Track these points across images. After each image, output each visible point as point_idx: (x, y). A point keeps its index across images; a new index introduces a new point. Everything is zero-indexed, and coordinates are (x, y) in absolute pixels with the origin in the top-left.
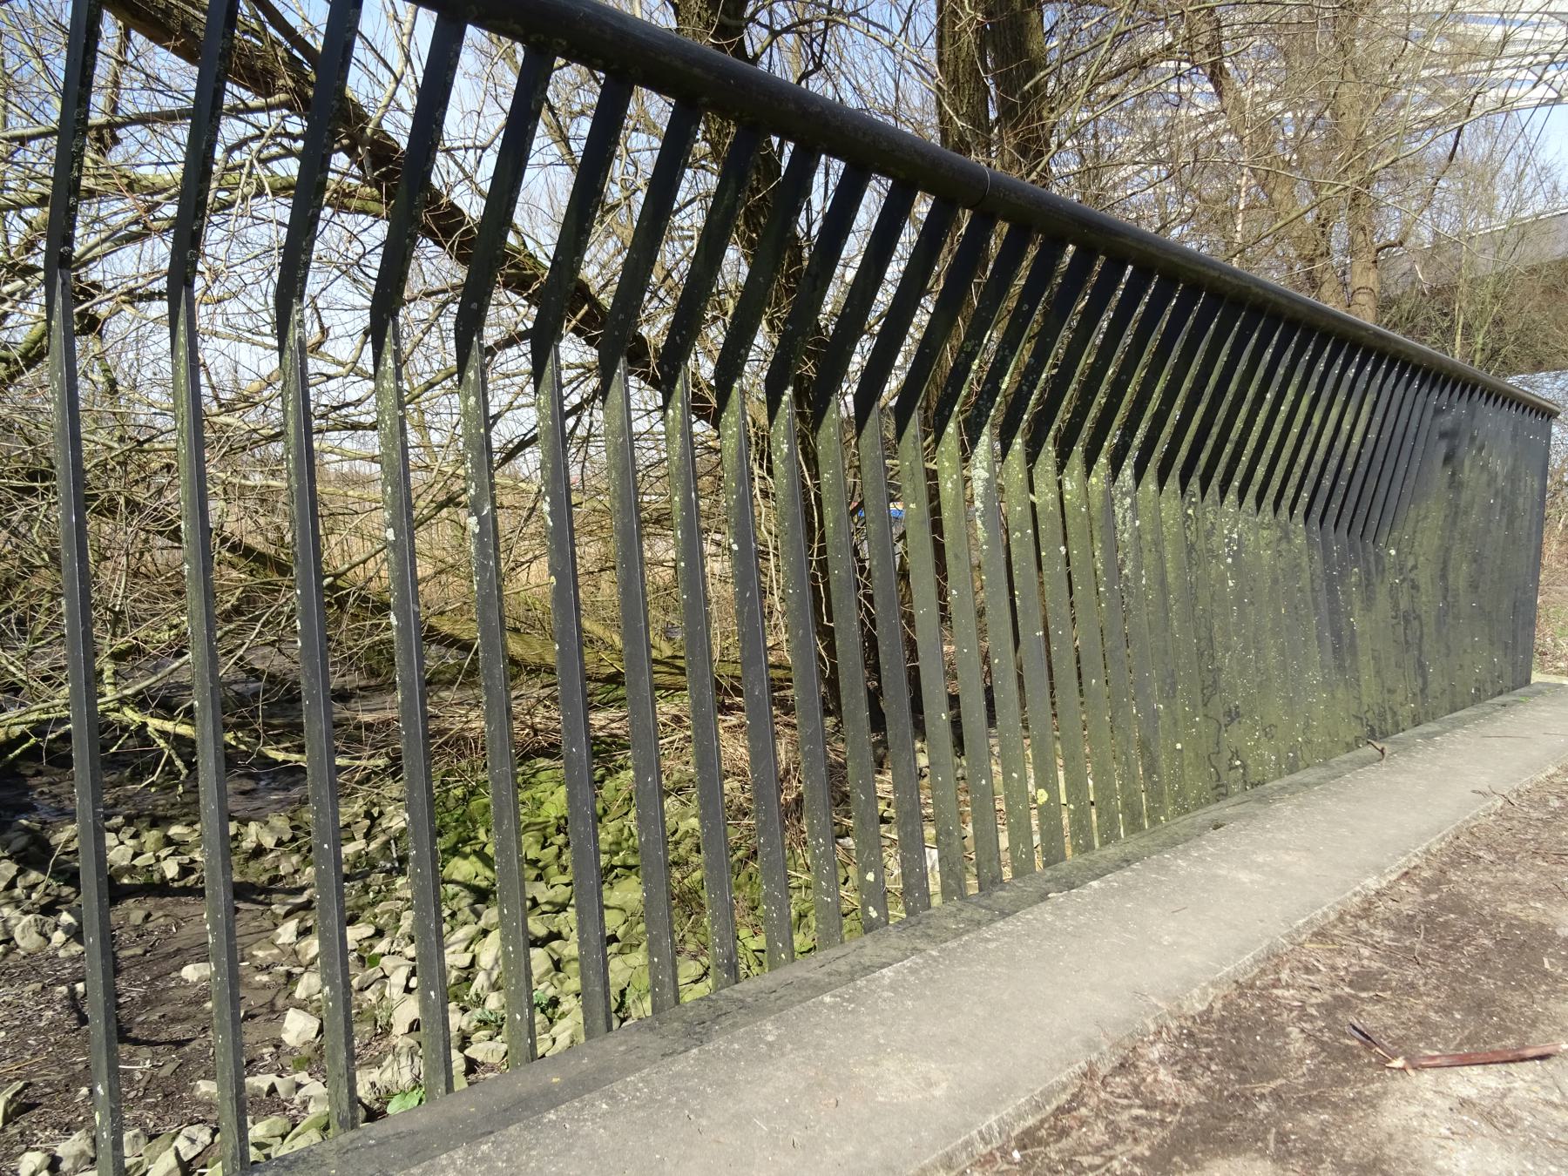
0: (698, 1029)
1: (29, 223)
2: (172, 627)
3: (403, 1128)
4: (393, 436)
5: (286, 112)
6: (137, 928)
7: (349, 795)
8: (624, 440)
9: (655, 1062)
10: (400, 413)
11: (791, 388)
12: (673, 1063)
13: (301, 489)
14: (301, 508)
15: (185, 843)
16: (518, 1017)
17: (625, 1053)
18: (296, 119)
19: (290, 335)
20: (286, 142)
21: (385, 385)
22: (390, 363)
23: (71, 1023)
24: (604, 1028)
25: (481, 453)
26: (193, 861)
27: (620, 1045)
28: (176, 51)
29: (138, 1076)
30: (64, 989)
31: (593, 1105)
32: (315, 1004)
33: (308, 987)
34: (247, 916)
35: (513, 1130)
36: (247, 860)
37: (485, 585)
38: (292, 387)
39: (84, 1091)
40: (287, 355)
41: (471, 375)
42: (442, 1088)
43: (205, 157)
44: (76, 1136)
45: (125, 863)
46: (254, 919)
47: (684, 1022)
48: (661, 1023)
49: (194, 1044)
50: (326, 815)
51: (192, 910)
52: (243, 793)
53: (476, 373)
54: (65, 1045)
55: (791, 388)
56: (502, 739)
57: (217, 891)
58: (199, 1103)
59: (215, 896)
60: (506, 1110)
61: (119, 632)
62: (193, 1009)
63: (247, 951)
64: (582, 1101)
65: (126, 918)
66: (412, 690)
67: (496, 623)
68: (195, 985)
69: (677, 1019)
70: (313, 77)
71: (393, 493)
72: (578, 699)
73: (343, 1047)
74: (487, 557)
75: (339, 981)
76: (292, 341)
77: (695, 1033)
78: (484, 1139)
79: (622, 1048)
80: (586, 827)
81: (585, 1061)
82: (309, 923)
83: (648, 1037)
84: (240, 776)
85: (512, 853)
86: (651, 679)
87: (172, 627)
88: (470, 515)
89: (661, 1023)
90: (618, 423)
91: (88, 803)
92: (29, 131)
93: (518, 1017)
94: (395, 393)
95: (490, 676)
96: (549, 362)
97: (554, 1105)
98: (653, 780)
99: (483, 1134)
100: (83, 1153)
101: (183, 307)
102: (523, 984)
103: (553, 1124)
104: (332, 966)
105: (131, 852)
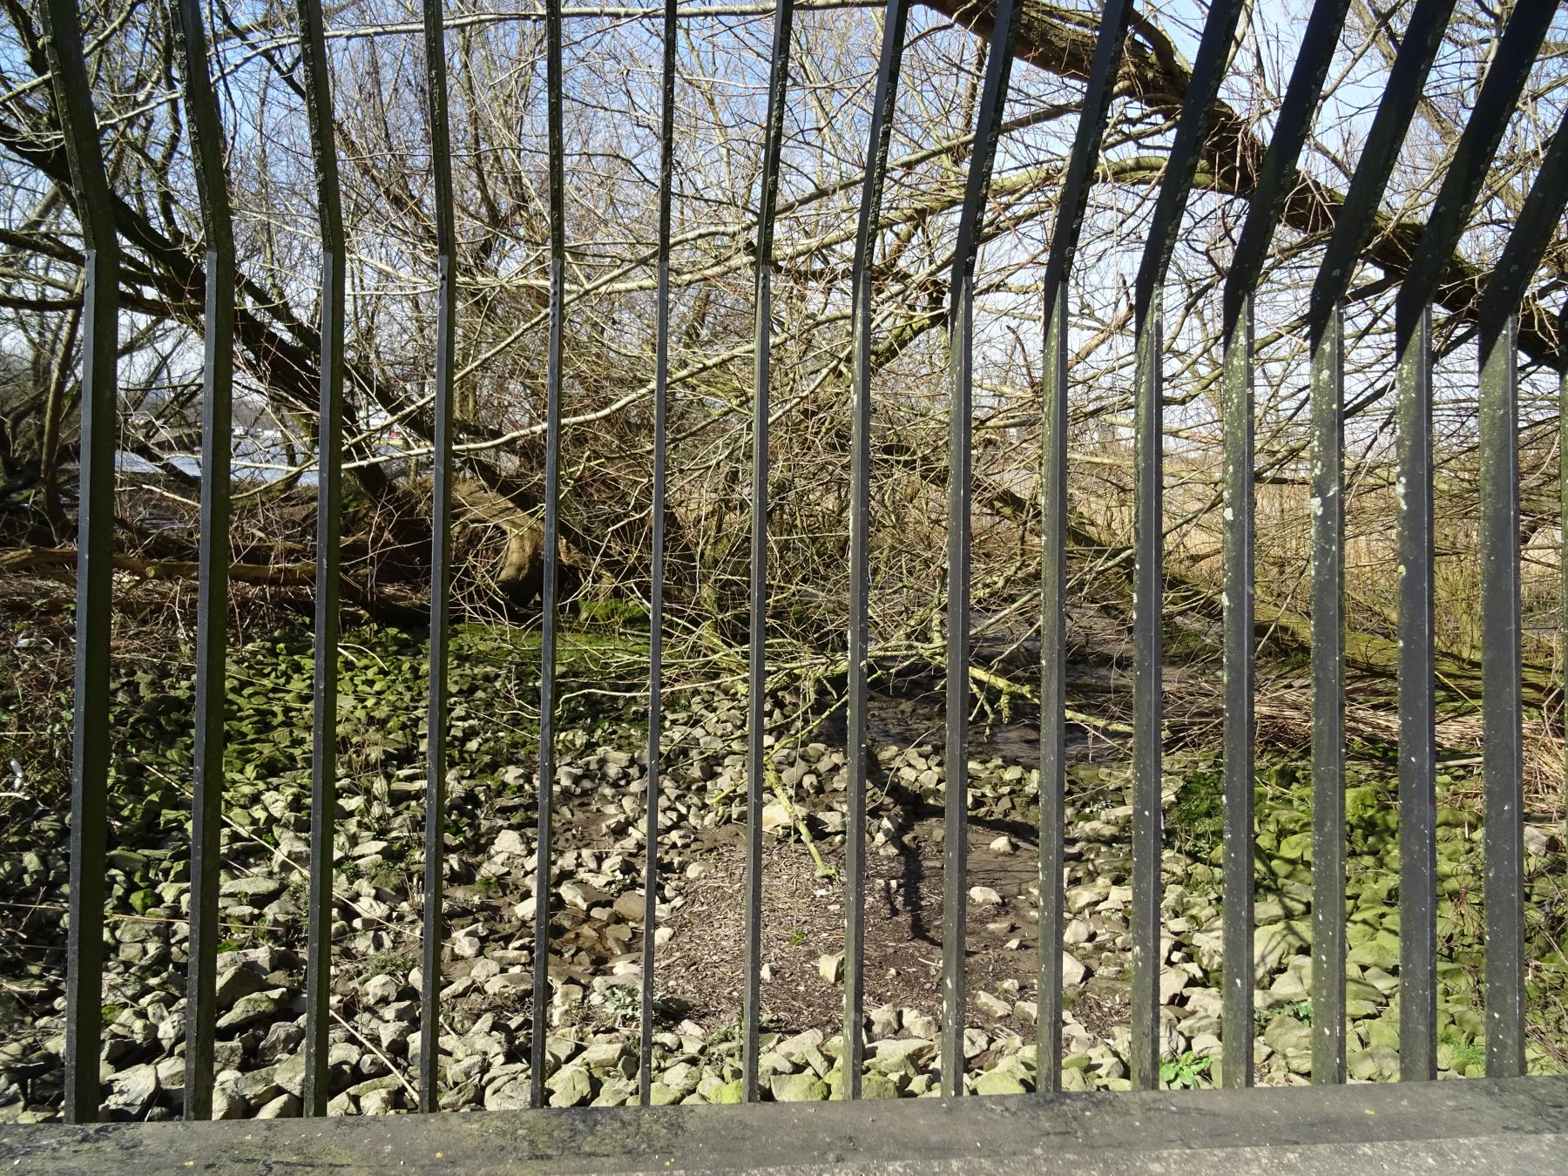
0: (1552, 1111)
1: (897, 235)
2: (986, 586)
3: (1203, 1105)
4: (1240, 414)
5: (1127, 99)
6: (937, 844)
7: (1122, 760)
8: (1506, 413)
9: (1494, 1132)
10: (1249, 391)
11: (119, 236)
12: (1520, 1141)
13: (1147, 468)
14: (1147, 486)
15: (978, 778)
16: (1327, 1032)
17: (1454, 1109)
18: (1137, 104)
19: (1148, 319)
20: (1125, 128)
21: (1235, 362)
22: (1242, 340)
23: (885, 912)
24: (1426, 1074)
25: (1332, 431)
26: (984, 795)
27: (1449, 1098)
28: (1035, 62)
29: (933, 972)
30: (882, 882)
31: (1417, 1155)
32: (1081, 952)
33: (1075, 934)
34: (1026, 855)
35: (1322, 1148)
36: (1028, 804)
37: (1324, 571)
38: (1146, 369)
39: (893, 971)
40: (1144, 338)
41: (1327, 347)
42: (1241, 1079)
43: (1090, 158)
44: (885, 1007)
45: (932, 786)
46: (1032, 858)
47: (1533, 1097)
48: (1502, 1090)
49: (977, 957)
50: (1149, 784)
51: (981, 839)
52: (1028, 742)
53: (1332, 345)
54: (879, 929)
55: (119, 236)
56: (1331, 737)
57: (953, 813)
58: (979, 1011)
59: (1048, 839)
60: (1312, 1125)
61: (1540, 661)
62: (978, 926)
63: (1024, 886)
64: (1403, 1146)
65: (930, 834)
66: (1240, 673)
67: (1334, 612)
68: (980, 905)
69: (1524, 1092)
70: (1153, 59)
71: (1235, 472)
72: (1424, 704)
73: (1149, 1008)
74: (1330, 541)
75: (1151, 944)
76: (1149, 325)
77: (1549, 1116)
78: (1291, 1147)
79: (1451, 1103)
80: (1421, 847)
81: (1405, 1102)
82: (1080, 874)
83: (1485, 1101)
84: (1026, 726)
85: (1334, 857)
86: (1519, 693)
87: (986, 586)
88: (1313, 496)
89: (1502, 1090)
90: (1498, 392)
91: (957, 738)
92: (913, 157)
93: (1327, 1032)
94: (1245, 370)
95: (1322, 667)
96: (1418, 327)
97: (1370, 1139)
98: (1511, 810)
99: (1288, 1142)
100: (889, 1023)
101: (1058, 300)
102: (1335, 998)
103: (1369, 1160)
104: (1144, 928)
105: (936, 777)
